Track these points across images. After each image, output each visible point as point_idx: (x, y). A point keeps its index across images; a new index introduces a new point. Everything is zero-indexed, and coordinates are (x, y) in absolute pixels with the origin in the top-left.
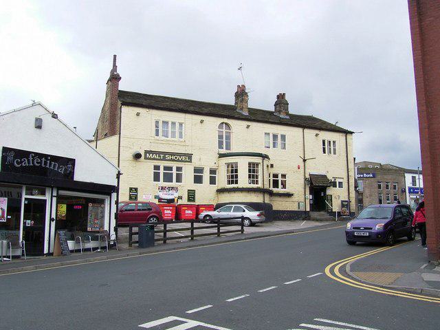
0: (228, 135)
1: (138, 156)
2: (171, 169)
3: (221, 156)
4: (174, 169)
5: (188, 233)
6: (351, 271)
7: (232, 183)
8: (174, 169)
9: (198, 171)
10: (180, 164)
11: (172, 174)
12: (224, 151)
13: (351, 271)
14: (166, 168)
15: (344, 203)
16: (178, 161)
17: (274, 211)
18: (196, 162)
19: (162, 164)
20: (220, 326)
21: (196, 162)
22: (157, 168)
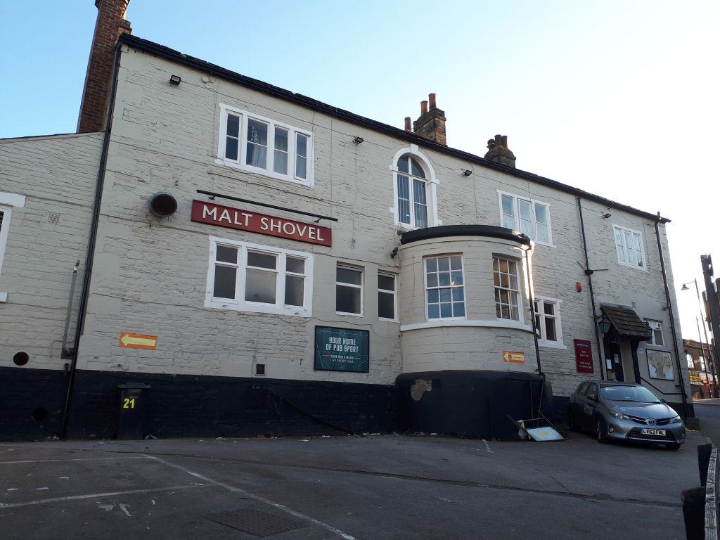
0: (584, 364)
1: (162, 206)
2: (269, 261)
3: (408, 237)
4: (281, 264)
5: (259, 351)
6: (599, 323)
7: (446, 314)
8: (281, 264)
9: (348, 272)
10: (298, 252)
11: (234, 270)
12: (411, 226)
13: (599, 323)
14: (255, 258)
15: (334, 342)
16: (295, 239)
17: (609, 331)
18: (341, 248)
19: (244, 245)
20: (317, 383)
21: (341, 248)
22: (227, 253)
